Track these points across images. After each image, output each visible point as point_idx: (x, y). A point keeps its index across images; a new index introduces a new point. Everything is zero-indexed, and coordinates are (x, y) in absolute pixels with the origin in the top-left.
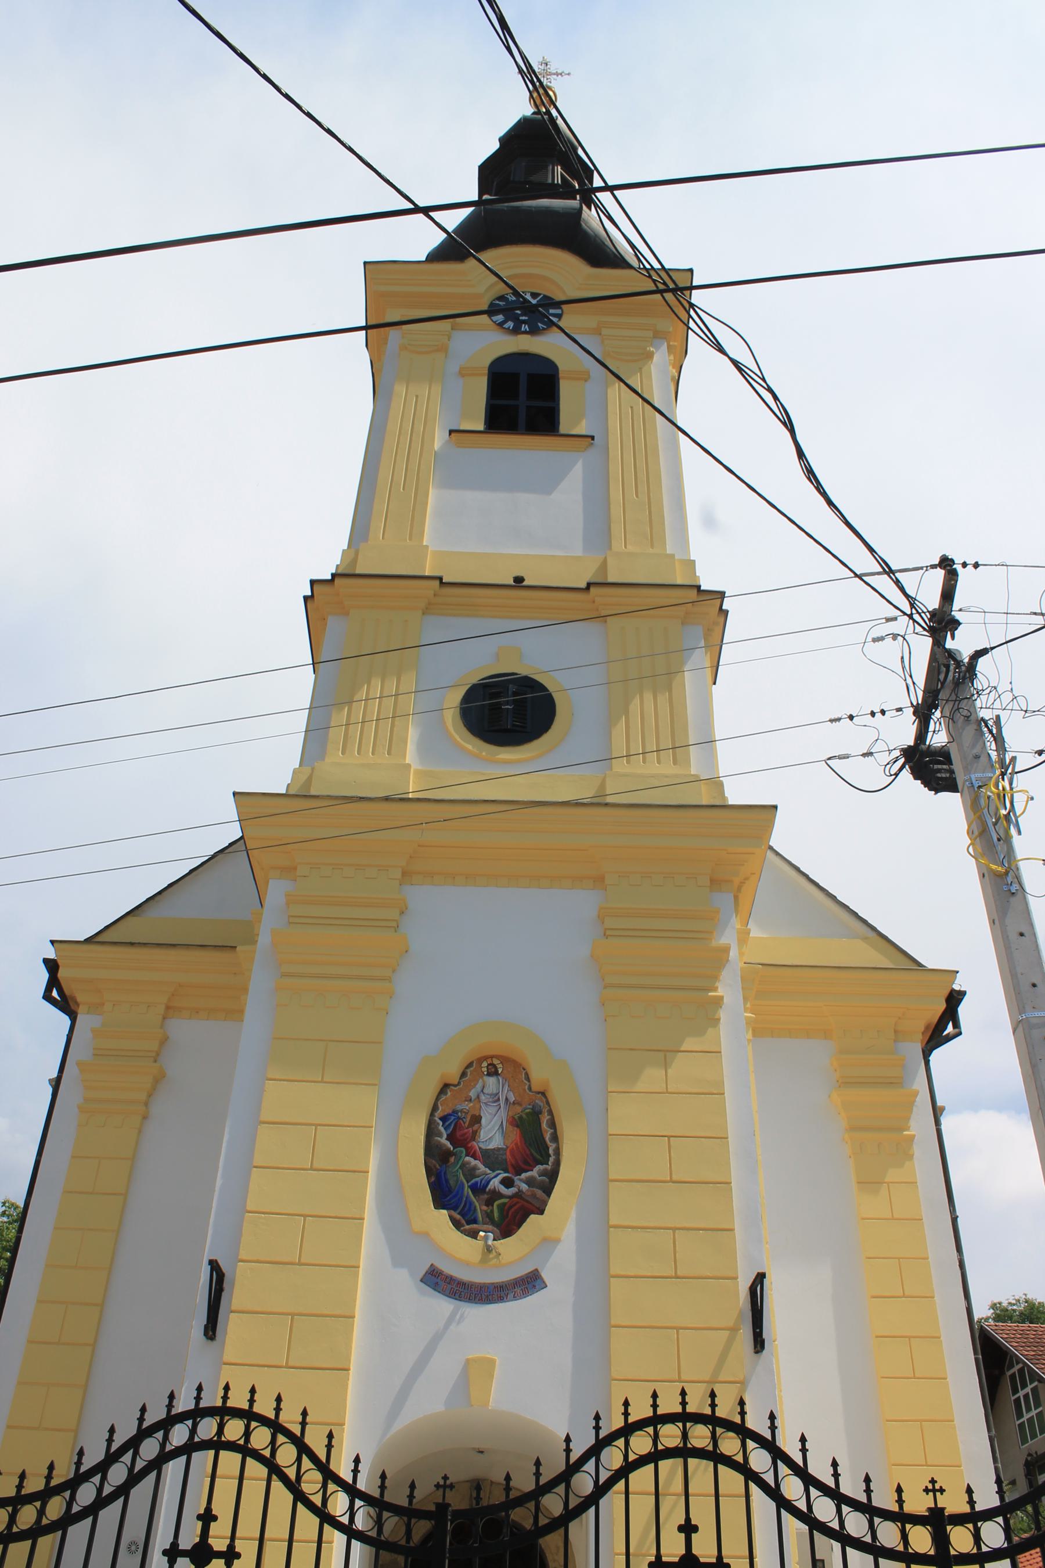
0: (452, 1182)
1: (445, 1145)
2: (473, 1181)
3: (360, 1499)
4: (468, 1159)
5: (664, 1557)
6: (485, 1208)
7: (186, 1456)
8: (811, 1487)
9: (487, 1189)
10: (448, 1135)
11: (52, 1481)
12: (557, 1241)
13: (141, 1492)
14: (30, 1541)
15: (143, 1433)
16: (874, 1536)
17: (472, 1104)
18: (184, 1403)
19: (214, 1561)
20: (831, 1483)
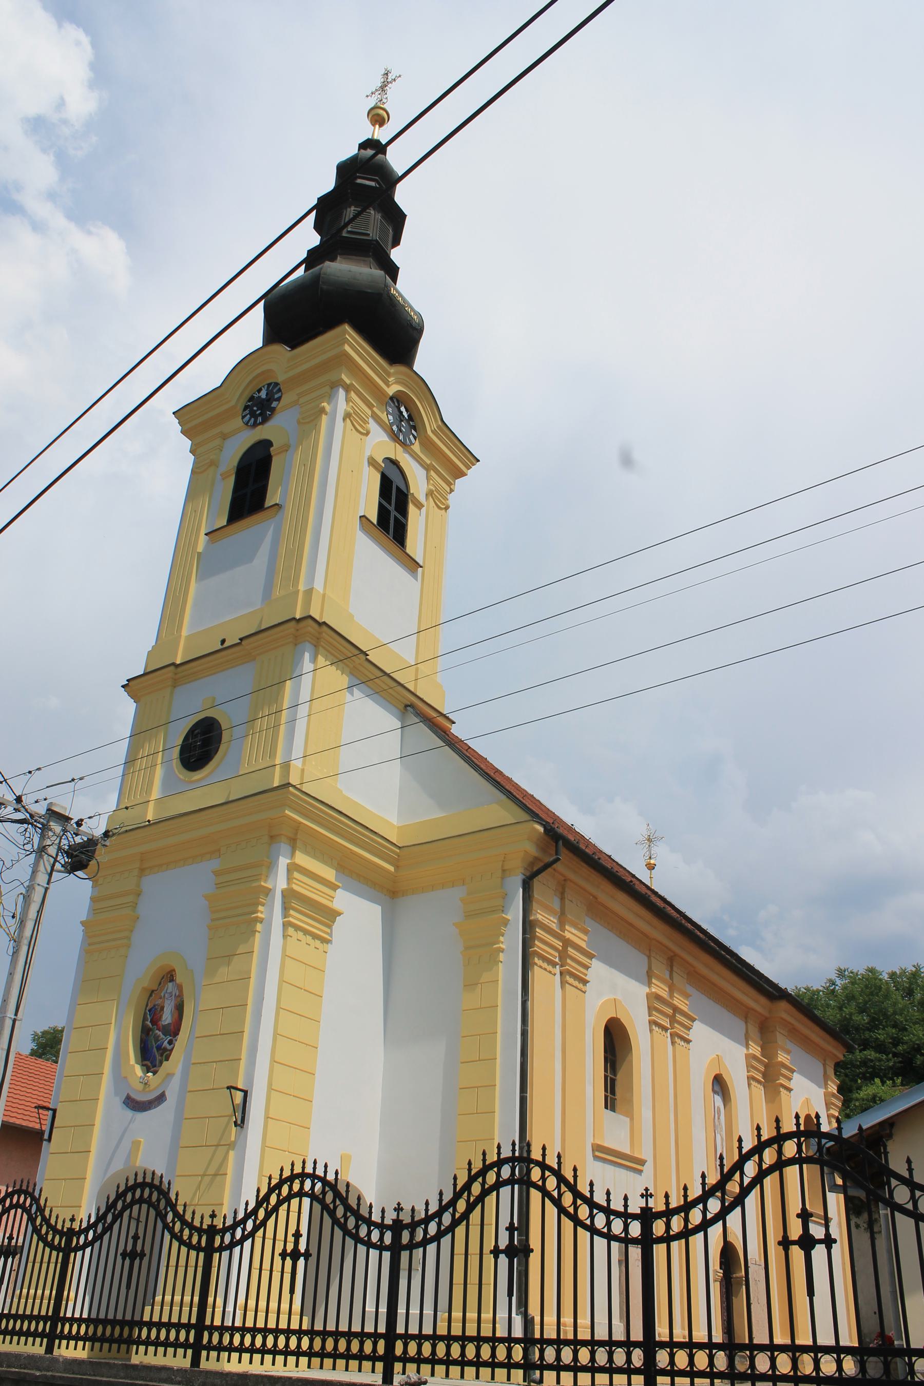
0: (149, 1046)
1: (148, 1025)
2: (157, 1044)
3: (596, 1209)
4: (157, 1031)
5: (679, 1243)
6: (160, 1058)
7: (778, 1172)
8: (546, 1198)
9: (162, 1047)
10: (151, 1020)
11: (429, 1211)
12: (173, 1074)
13: (475, 1216)
14: (702, 1232)
15: (472, 1179)
16: (609, 1229)
17: (161, 1000)
18: (492, 1157)
19: (797, 1239)
20: (906, 1175)
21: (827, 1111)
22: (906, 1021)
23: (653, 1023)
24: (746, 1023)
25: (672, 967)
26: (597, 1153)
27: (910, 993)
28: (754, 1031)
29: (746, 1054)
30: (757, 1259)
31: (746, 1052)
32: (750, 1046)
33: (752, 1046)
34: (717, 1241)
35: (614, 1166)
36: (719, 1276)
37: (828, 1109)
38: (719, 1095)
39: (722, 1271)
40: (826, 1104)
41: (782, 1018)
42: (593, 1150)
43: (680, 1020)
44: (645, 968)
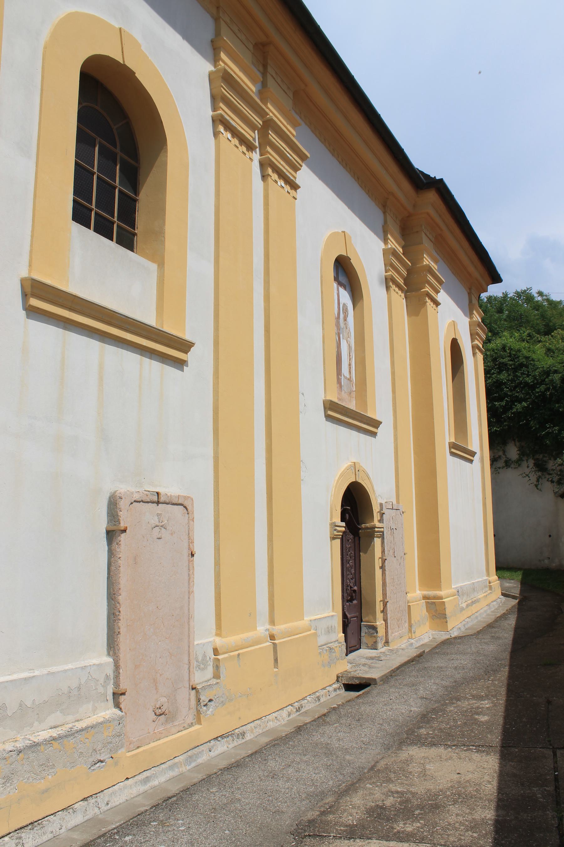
21: (472, 342)
22: (499, 328)
23: (218, 121)
24: (384, 213)
25: (265, 66)
26: (34, 302)
27: (500, 311)
28: (393, 227)
29: (384, 250)
30: (395, 502)
31: (384, 247)
32: (389, 241)
33: (392, 242)
34: (338, 481)
35: (141, 355)
36: (339, 531)
37: (472, 340)
38: (345, 290)
39: (343, 524)
40: (471, 335)
41: (428, 214)
42: (325, 408)
43: (278, 144)
44: (209, 34)
